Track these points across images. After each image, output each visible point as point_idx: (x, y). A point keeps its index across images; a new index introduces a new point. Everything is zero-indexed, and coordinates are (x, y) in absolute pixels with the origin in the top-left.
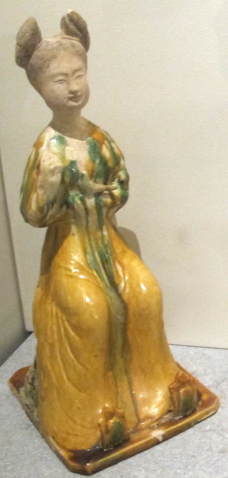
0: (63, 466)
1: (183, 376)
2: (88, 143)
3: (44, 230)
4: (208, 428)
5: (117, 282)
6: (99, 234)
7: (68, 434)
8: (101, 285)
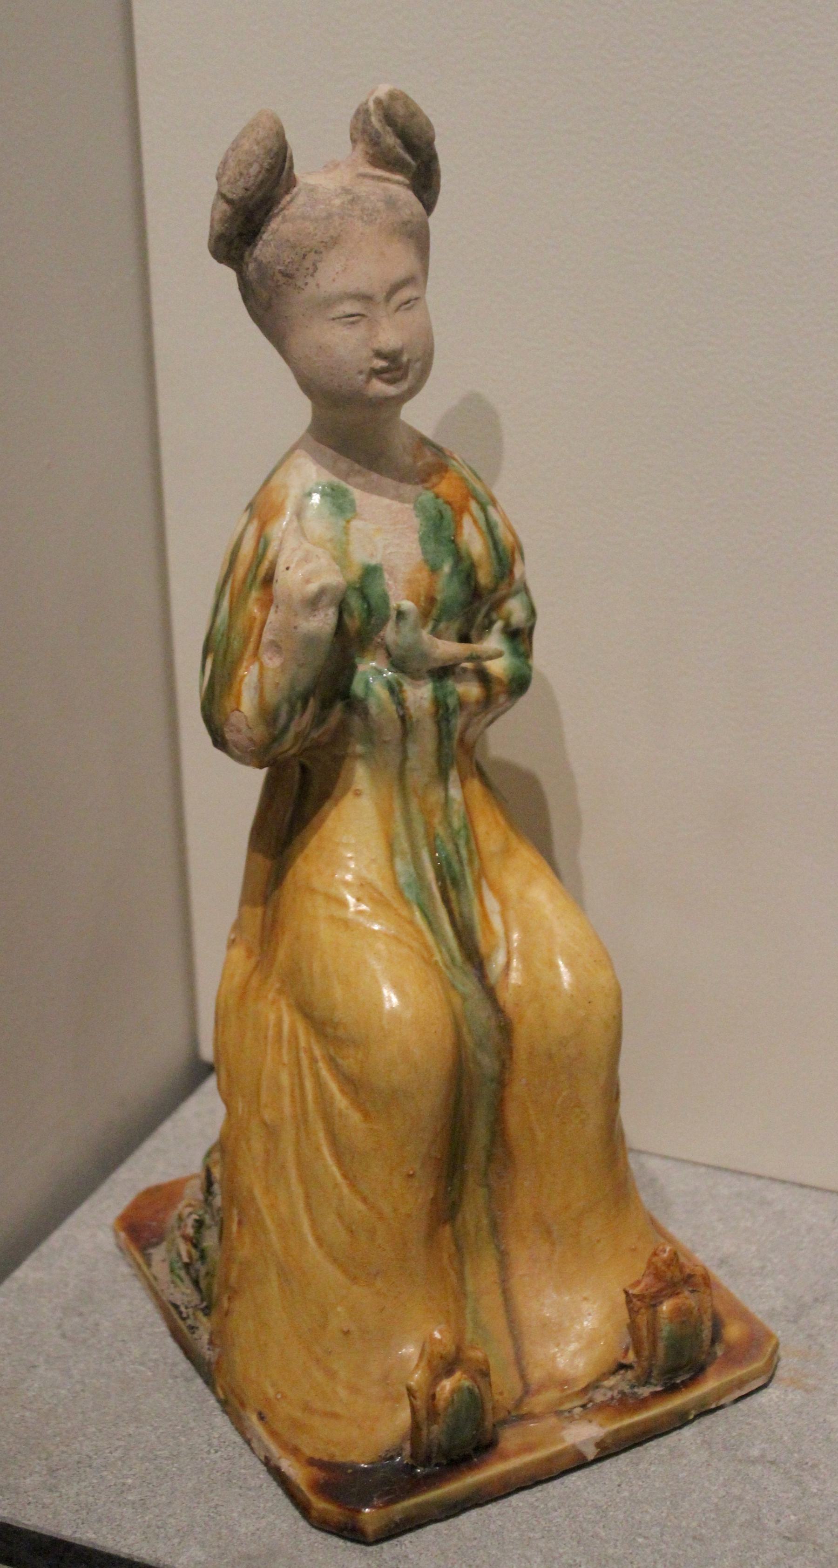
0: (294, 1513)
1: (674, 1260)
2: (421, 509)
3: (265, 771)
4: (755, 1452)
5: (483, 948)
6: (435, 796)
7: (307, 1408)
8: (437, 957)
